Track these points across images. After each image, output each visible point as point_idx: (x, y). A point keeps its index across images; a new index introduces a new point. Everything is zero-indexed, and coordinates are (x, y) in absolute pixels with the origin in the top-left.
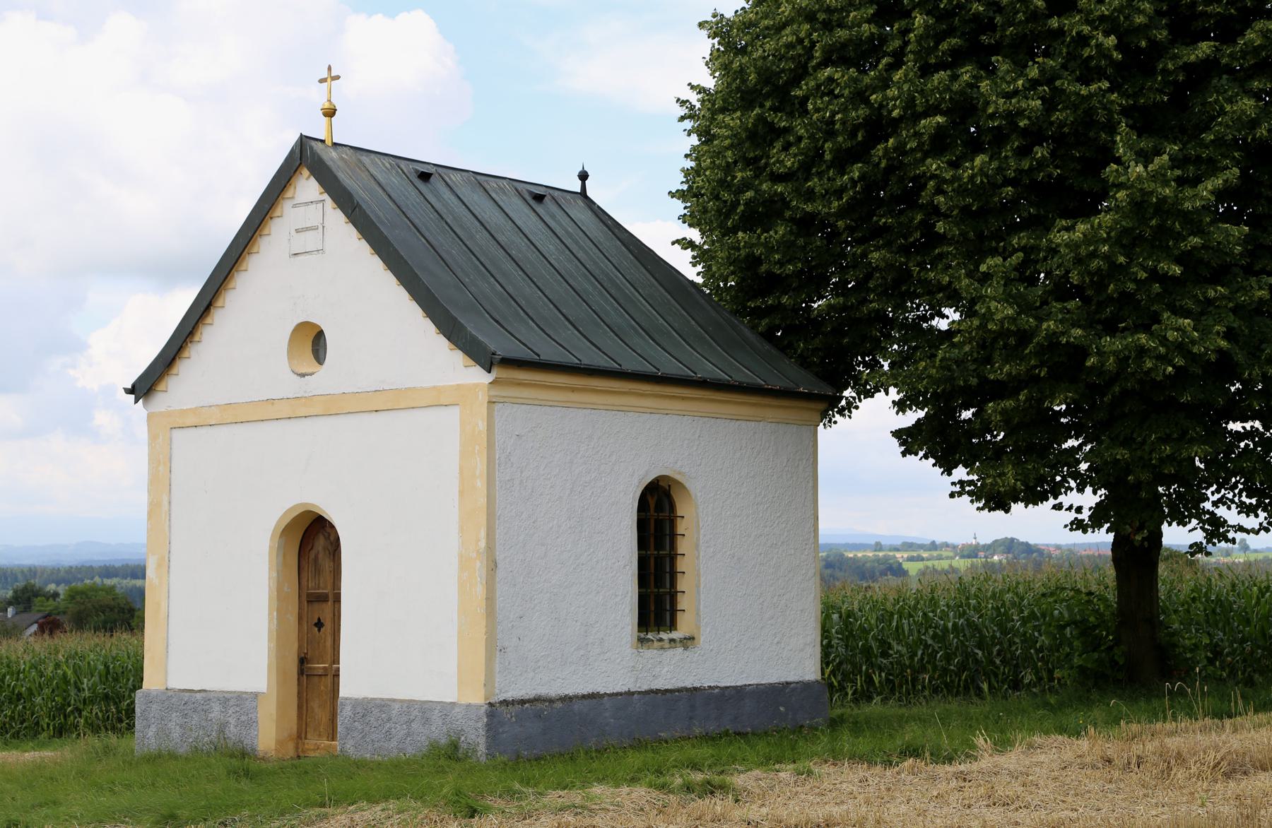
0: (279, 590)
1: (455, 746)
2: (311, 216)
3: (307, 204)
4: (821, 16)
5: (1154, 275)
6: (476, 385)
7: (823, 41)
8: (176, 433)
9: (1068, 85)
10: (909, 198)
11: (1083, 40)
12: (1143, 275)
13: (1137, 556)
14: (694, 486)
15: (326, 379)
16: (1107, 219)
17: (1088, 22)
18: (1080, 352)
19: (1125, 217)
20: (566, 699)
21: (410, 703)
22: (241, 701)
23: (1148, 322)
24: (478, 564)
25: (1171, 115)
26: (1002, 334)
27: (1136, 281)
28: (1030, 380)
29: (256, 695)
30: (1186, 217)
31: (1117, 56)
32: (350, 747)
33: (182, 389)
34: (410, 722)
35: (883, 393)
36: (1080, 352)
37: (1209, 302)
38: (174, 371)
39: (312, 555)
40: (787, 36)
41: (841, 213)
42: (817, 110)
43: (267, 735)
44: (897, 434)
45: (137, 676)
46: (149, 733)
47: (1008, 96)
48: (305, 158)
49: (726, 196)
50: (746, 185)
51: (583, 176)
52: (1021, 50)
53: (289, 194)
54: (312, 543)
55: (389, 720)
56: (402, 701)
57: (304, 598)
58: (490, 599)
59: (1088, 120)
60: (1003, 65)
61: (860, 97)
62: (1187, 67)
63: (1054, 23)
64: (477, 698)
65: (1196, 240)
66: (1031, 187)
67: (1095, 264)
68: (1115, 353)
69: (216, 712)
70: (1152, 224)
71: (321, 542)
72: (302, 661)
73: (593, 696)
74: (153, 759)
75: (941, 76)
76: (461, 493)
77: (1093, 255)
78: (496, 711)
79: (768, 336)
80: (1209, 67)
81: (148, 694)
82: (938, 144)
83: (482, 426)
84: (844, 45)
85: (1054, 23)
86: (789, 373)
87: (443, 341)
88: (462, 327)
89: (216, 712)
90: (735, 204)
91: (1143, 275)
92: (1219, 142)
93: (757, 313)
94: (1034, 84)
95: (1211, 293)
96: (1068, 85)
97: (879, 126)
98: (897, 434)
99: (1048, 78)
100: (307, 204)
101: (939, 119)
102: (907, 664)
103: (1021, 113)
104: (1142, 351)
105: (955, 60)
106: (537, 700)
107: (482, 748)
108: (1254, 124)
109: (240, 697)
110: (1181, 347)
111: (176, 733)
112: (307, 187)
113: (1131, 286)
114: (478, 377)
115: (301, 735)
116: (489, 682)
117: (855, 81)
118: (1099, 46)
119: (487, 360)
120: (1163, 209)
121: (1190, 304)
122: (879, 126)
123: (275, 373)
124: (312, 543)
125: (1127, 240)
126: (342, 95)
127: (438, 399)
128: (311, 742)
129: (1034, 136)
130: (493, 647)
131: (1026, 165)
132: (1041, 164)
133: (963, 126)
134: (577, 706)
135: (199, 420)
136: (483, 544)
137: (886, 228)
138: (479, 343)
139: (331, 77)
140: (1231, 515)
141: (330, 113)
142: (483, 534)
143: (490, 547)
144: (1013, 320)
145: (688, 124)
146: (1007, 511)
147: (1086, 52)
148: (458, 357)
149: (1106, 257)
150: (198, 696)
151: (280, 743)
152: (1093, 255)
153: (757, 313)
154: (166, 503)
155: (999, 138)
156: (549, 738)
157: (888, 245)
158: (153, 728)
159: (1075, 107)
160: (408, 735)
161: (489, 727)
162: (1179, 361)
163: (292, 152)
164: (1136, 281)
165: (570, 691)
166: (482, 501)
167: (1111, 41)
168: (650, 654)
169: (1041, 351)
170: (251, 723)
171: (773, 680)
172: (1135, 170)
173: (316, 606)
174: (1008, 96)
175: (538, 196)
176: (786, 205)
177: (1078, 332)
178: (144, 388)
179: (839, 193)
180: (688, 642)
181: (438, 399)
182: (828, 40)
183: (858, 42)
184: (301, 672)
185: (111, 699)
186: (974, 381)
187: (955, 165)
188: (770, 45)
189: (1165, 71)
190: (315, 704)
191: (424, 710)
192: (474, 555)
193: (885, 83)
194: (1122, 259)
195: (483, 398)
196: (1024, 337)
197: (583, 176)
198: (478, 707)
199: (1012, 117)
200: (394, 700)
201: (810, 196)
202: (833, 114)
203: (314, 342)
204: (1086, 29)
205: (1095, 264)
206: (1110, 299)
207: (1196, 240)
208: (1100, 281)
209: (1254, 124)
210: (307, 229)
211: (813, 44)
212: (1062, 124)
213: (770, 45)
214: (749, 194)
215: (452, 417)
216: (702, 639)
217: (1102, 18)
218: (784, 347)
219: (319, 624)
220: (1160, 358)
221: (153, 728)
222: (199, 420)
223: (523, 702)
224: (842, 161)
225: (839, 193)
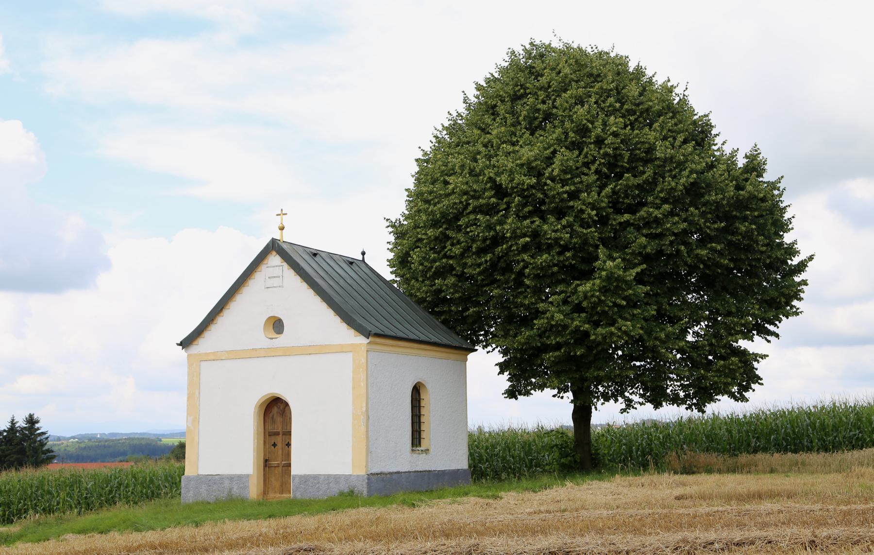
0: (133, 439)
1: (352, 492)
2: (277, 272)
4: (472, 193)
5: (615, 304)
7: (473, 203)
8: (203, 363)
9: (577, 228)
10: (508, 269)
11: (582, 211)
12: (611, 304)
13: (582, 414)
14: (429, 386)
15: (282, 340)
16: (598, 282)
17: (584, 204)
18: (586, 334)
19: (604, 281)
20: (391, 473)
21: (329, 476)
22: (241, 479)
23: (613, 323)
25: (615, 243)
26: (557, 325)
27: (608, 306)
28: (566, 344)
29: (248, 476)
30: (626, 282)
31: (596, 218)
32: (298, 496)
33: (203, 345)
34: (328, 484)
36: (586, 334)
37: (634, 315)
38: (203, 336)
39: (271, 415)
40: (454, 199)
41: (480, 274)
42: (471, 231)
43: (253, 491)
46: (188, 494)
47: (554, 231)
48: (274, 247)
49: (426, 264)
50: (434, 261)
51: (363, 254)
52: (560, 213)
53: (265, 262)
54: (275, 411)
57: (267, 434)
58: (367, 431)
59: (585, 242)
60: (551, 219)
61: (490, 227)
62: (620, 223)
63: (571, 203)
64: (362, 472)
65: (631, 292)
66: (562, 267)
67: (594, 299)
68: (602, 335)
69: (227, 484)
70: (613, 286)
71: (275, 410)
72: (266, 461)
73: (398, 473)
74: (189, 507)
75: (527, 222)
76: (354, 388)
77: (593, 296)
78: (370, 476)
79: (445, 322)
80: (627, 224)
81: (188, 477)
82: (525, 248)
83: (364, 360)
84: (481, 206)
85: (571, 203)
86: (457, 341)
87: (344, 326)
88: (355, 320)
89: (227, 484)
90: (432, 267)
91: (611, 304)
92: (633, 253)
93: (440, 314)
94: (564, 227)
95: (635, 312)
96: (577, 228)
97: (497, 240)
99: (570, 225)
101: (528, 239)
102: (499, 462)
103: (561, 238)
104: (612, 334)
105: (531, 214)
106: (381, 473)
107: (365, 493)
108: (645, 247)
109: (240, 477)
110: (625, 333)
112: (274, 260)
113: (607, 309)
114: (362, 340)
115: (265, 492)
116: (367, 466)
117: (488, 220)
118: (589, 214)
119: (367, 334)
120: (619, 279)
121: (627, 316)
122: (497, 240)
123: (261, 339)
124: (275, 411)
125: (604, 290)
126: (286, 221)
127: (341, 349)
128: (271, 495)
129: (565, 248)
130: (369, 452)
131: (561, 258)
132: (568, 259)
133: (538, 243)
134: (394, 476)
135: (215, 357)
136: (364, 409)
137: (499, 280)
138: (363, 327)
139: (282, 214)
140: (636, 398)
141: (282, 229)
142: (364, 405)
143: (367, 411)
144: (562, 320)
145: (390, 229)
146: (516, 399)
147: (584, 216)
148: (352, 332)
149: (597, 297)
151: (258, 496)
152: (593, 296)
153: (440, 314)
154: (197, 393)
155: (549, 247)
156: (386, 487)
157: (499, 287)
158: (191, 492)
159: (580, 237)
161: (368, 484)
162: (625, 338)
163: (268, 245)
164: (608, 306)
165: (391, 471)
166: (364, 391)
167: (594, 212)
168: (415, 456)
169: (572, 332)
170: (246, 487)
171: (453, 468)
172: (609, 264)
173: (273, 437)
174: (554, 231)
175: (351, 262)
176: (454, 269)
177: (587, 326)
178: (185, 344)
179: (479, 265)
180: (427, 451)
181: (341, 349)
182: (476, 203)
183: (488, 205)
184: (265, 466)
185: (174, 482)
186: (539, 344)
187: (532, 257)
188: (446, 202)
189: (612, 225)
190: (273, 479)
191: (337, 478)
193: (501, 223)
194: (603, 298)
195: (364, 349)
196: (565, 327)
197: (363, 254)
198: (363, 476)
199: (557, 240)
201: (465, 265)
202: (479, 233)
203: (277, 325)
204: (584, 207)
205: (594, 299)
206: (597, 313)
207: (631, 292)
208: (594, 306)
209: (645, 247)
211: (469, 204)
212: (575, 244)
213: (446, 202)
214: (437, 264)
216: (431, 451)
217: (590, 203)
218: (452, 328)
219: (274, 445)
220: (618, 336)
221: (191, 492)
222: (215, 357)
223: (377, 474)
224: (481, 251)
225: (479, 265)
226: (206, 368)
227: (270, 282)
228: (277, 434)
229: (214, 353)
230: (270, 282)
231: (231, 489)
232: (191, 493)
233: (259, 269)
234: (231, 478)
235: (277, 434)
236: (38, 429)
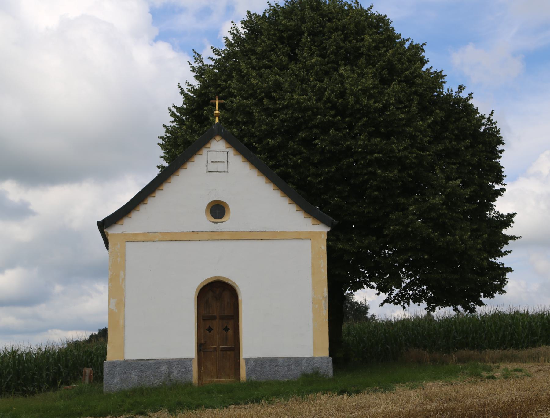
2: (222, 157)
3: (217, 151)
6: (320, 232)
8: (129, 245)
15: (227, 224)
21: (289, 359)
22: (182, 363)
24: (323, 302)
35: (163, 155)
44: (503, 144)
45: (104, 356)
46: (113, 383)
53: (208, 146)
55: (277, 366)
56: (282, 358)
69: (164, 369)
76: (313, 274)
81: (114, 364)
98: (503, 144)
100: (217, 151)
103: (407, 157)
109: (181, 362)
111: (135, 379)
127: (298, 236)
150: (150, 362)
160: (288, 371)
181: (298, 236)
191: (298, 361)
192: (321, 298)
200: (279, 358)
202: (325, 147)
210: (219, 162)
215: (307, 244)
225: (321, 175)
226: (133, 250)
227: (212, 167)
228: (214, 318)
229: (144, 234)
230: (212, 167)
231: (170, 374)
232: (117, 380)
233: (200, 153)
234: (170, 363)
235: (214, 318)
236: (409, 305)
